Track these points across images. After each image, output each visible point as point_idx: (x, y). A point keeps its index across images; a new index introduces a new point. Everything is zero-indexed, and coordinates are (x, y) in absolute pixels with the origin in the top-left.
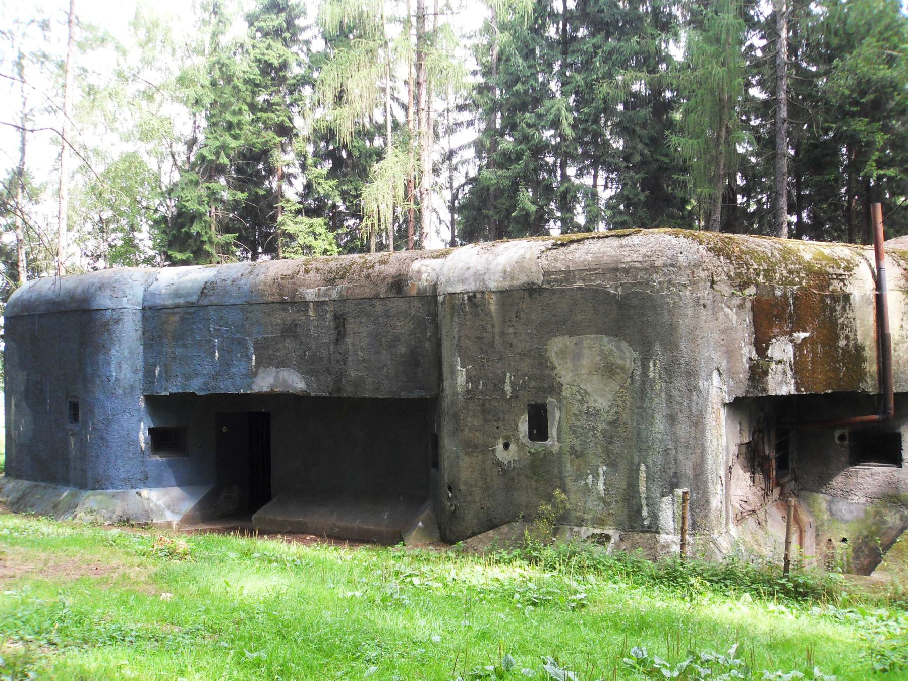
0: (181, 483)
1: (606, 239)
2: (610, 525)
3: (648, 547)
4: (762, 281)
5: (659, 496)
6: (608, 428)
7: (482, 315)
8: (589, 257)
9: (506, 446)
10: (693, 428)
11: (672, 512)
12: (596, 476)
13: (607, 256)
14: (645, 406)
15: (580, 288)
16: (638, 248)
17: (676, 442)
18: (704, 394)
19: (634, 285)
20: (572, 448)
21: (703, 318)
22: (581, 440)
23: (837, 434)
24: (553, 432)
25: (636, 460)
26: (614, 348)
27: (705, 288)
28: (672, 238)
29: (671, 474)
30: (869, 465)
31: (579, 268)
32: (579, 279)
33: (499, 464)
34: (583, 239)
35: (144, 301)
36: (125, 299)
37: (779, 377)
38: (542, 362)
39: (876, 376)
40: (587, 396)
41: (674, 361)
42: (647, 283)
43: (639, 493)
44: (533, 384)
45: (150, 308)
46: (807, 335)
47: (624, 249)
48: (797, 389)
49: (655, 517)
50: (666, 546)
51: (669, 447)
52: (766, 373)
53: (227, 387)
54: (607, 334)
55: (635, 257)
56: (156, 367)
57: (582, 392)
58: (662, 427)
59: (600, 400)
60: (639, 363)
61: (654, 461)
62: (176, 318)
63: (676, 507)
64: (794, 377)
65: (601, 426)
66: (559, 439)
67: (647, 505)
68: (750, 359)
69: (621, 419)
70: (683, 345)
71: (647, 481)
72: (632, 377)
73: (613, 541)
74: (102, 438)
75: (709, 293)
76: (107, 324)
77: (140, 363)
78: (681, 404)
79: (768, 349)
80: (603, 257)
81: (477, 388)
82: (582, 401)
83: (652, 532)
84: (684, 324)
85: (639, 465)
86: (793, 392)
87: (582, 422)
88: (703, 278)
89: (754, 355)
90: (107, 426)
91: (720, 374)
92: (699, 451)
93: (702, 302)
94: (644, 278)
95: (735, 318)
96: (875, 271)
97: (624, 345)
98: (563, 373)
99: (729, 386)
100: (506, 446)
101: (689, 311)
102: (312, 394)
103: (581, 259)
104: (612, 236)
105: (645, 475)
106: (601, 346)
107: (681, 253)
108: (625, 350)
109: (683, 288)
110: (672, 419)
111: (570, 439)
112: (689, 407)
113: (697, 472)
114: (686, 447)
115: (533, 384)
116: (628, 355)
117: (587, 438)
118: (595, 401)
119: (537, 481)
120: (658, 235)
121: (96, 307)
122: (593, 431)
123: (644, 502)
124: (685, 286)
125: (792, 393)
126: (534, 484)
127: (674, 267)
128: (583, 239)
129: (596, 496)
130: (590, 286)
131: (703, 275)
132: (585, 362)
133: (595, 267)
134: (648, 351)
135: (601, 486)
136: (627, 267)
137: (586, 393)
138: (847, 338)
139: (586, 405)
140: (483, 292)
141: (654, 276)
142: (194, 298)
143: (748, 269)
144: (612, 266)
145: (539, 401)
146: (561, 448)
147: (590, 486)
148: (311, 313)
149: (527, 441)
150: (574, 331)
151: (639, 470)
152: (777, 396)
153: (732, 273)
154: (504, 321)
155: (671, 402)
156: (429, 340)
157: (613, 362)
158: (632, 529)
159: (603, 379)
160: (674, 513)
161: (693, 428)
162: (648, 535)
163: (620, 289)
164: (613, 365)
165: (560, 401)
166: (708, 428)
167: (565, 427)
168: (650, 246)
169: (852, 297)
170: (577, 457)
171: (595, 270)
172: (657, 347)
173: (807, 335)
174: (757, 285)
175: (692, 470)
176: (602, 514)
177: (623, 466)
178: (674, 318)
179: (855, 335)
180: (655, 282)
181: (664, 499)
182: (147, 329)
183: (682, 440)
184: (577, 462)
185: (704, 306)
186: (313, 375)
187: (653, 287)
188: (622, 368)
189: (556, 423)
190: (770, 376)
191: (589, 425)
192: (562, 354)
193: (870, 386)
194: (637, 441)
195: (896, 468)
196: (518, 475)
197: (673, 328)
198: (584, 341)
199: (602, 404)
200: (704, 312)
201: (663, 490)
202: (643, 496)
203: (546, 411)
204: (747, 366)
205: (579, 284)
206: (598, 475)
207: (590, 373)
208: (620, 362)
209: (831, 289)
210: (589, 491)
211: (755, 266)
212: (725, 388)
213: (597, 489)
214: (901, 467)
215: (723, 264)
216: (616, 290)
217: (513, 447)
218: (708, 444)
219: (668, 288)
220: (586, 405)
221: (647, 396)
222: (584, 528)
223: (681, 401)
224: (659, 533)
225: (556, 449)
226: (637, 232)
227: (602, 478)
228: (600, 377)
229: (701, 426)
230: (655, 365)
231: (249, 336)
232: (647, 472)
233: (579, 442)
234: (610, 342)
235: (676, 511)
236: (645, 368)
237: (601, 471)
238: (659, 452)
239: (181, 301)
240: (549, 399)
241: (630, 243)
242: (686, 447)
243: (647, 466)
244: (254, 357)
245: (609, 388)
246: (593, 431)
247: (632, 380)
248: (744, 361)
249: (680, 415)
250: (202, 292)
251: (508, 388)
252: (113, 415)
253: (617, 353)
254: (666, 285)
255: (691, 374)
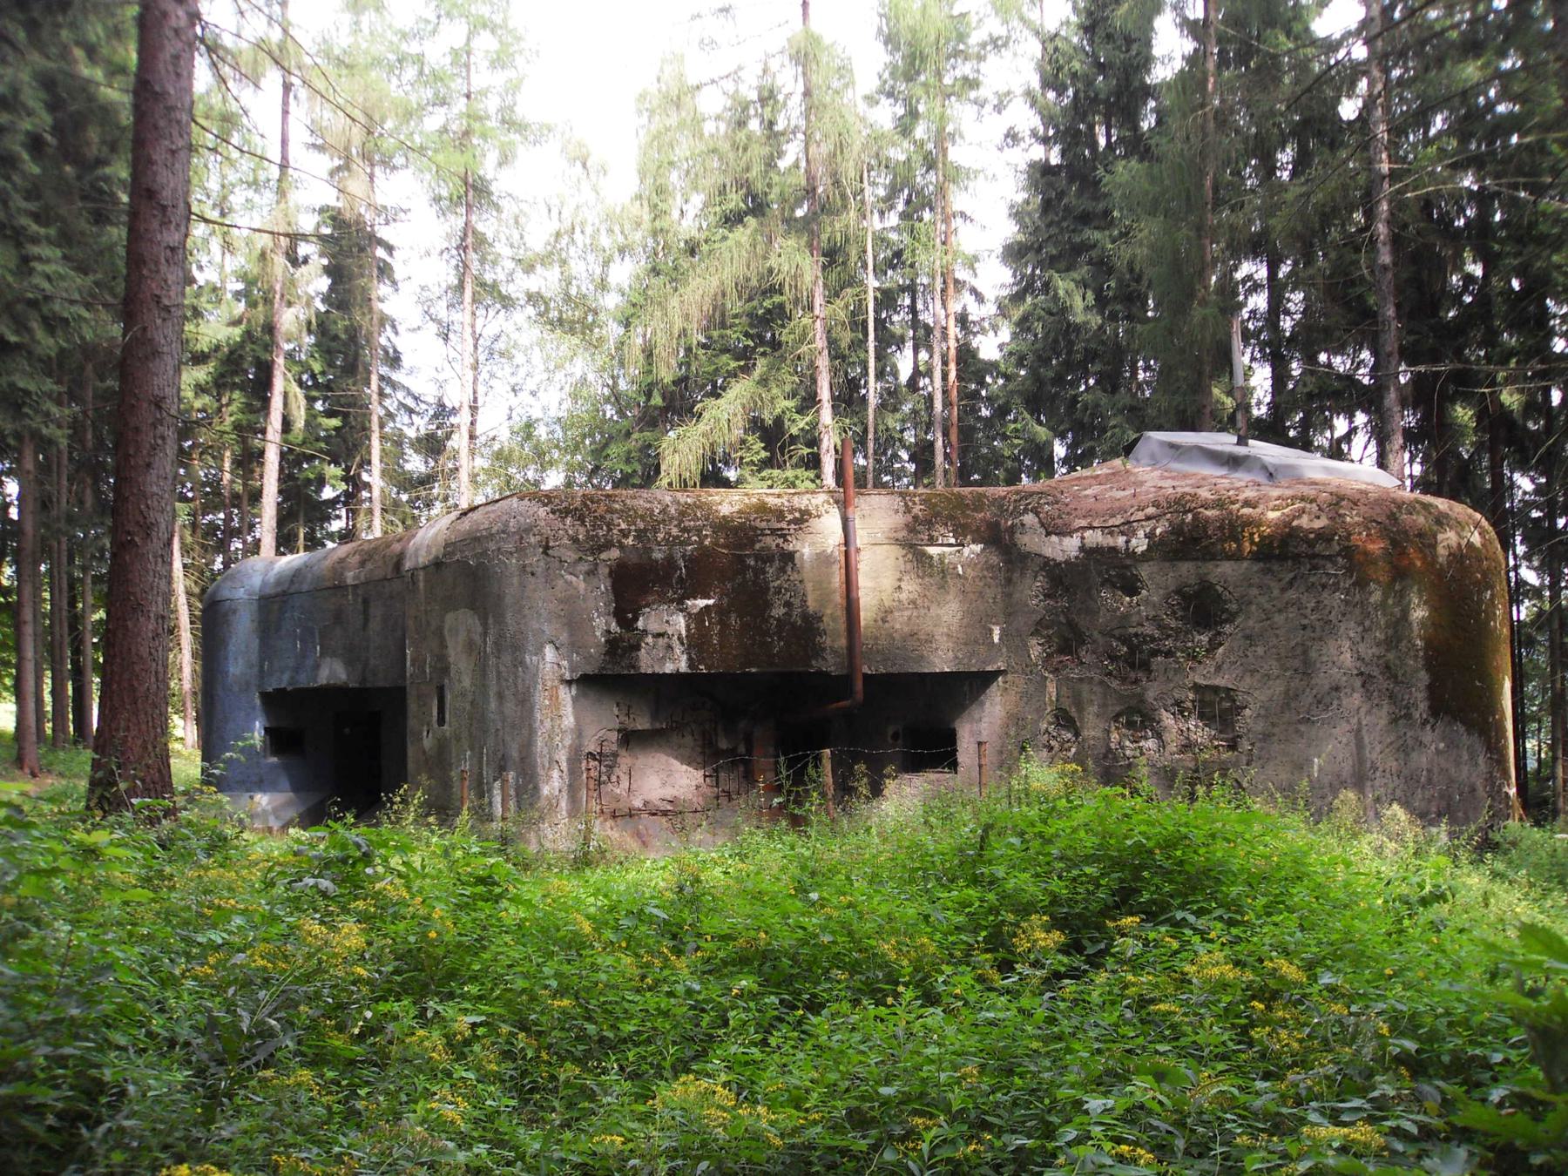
0: (296, 788)
41: (501, 636)
46: (711, 602)
53: (304, 681)
68: (608, 632)
76: (226, 615)
77: (254, 658)
84: (511, 590)
89: (614, 627)
92: (525, 732)
95: (582, 586)
99: (571, 662)
101: (515, 580)
110: (500, 696)
138: (788, 604)
143: (610, 530)
152: (654, 675)
173: (711, 602)
174: (622, 547)
197: (500, 598)
200: (531, 579)
209: (757, 546)
255: (517, 648)
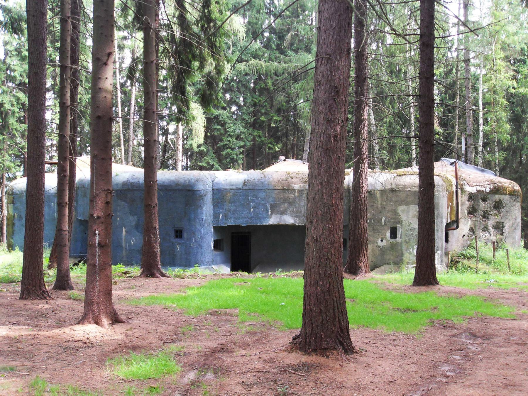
7: (374, 198)
9: (382, 241)
12: (413, 249)
20: (405, 241)
24: (399, 235)
33: (379, 247)
35: (213, 186)
36: (207, 186)
38: (395, 213)
44: (392, 221)
45: (217, 190)
56: (220, 214)
62: (231, 194)
66: (401, 238)
70: (440, 209)
74: (199, 245)
81: (371, 222)
87: (409, 232)
90: (202, 240)
98: (403, 217)
100: (382, 241)
102: (297, 225)
111: (405, 238)
115: (392, 221)
119: (393, 252)
121: (197, 189)
126: (392, 253)
137: (411, 223)
140: (374, 190)
142: (241, 186)
145: (394, 226)
146: (402, 241)
148: (296, 194)
149: (389, 239)
150: (407, 204)
154: (382, 200)
156: (346, 205)
165: (402, 226)
167: (403, 234)
170: (407, 243)
182: (215, 198)
184: (407, 244)
186: (297, 218)
189: (400, 233)
192: (403, 211)
196: (386, 250)
203: (396, 229)
205: (409, 189)
207: (412, 217)
217: (384, 241)
225: (400, 241)
231: (268, 202)
239: (234, 187)
240: (398, 225)
244: (270, 211)
250: (244, 184)
251: (383, 222)
252: (204, 235)
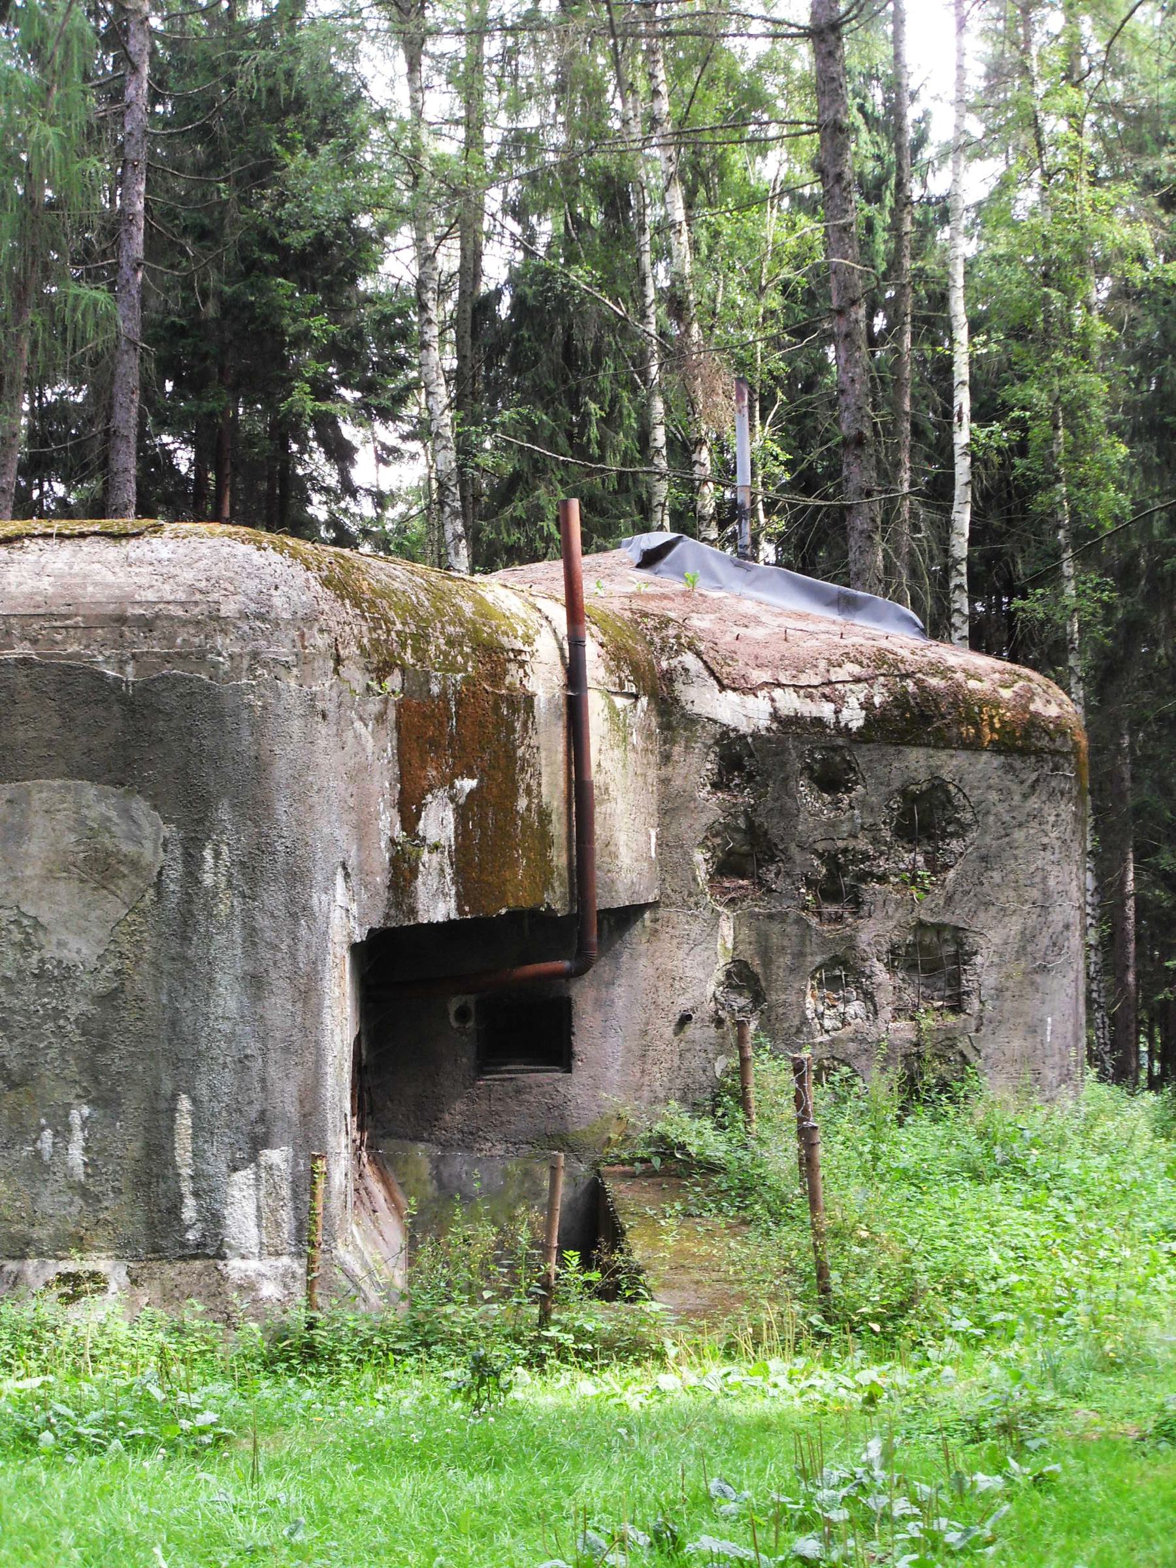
1: (83, 543)
2: (100, 1249)
3: (205, 1292)
4: (411, 661)
5: (224, 1169)
6: (92, 1010)
8: (46, 584)
10: (299, 1005)
11: (254, 1206)
12: (63, 1132)
13: (96, 584)
14: (190, 953)
15: (25, 662)
16: (177, 571)
17: (263, 1039)
18: (321, 920)
19: (167, 658)
21: (322, 743)
22: (22, 1044)
23: (453, 1005)
25: (167, 1087)
26: (113, 814)
27: (326, 674)
28: (249, 548)
29: (254, 1115)
30: (509, 1072)
31: (21, 611)
32: (23, 638)
34: (19, 537)
37: (433, 882)
39: (566, 874)
40: (41, 934)
41: (262, 848)
42: (202, 656)
43: (175, 1167)
47: (135, 569)
48: (460, 909)
49: (214, 1220)
50: (247, 1287)
51: (249, 1052)
52: (414, 872)
54: (93, 778)
55: (167, 591)
57: (26, 922)
58: (232, 1005)
59: (74, 943)
60: (178, 853)
61: (211, 1087)
63: (262, 1193)
64: (454, 882)
65: (79, 1007)
67: (196, 1194)
68: (392, 841)
69: (128, 988)
70: (281, 807)
71: (194, 1137)
72: (158, 886)
73: (113, 1287)
75: (331, 686)
78: (276, 948)
79: (419, 818)
80: (84, 586)
82: (27, 946)
83: (208, 1257)
85: (174, 1097)
86: (454, 915)
88: (323, 649)
89: (400, 835)
91: (347, 876)
93: (320, 705)
94: (191, 644)
95: (370, 744)
96: (566, 646)
97: (140, 806)
103: (26, 589)
104: (95, 534)
105: (189, 1122)
106: (79, 807)
107: (276, 588)
108: (144, 822)
109: (282, 672)
110: (255, 983)
112: (293, 957)
113: (307, 1109)
114: (286, 1050)
116: (148, 830)
117: (40, 1037)
118: (61, 944)
120: (216, 542)
122: (55, 1020)
123: (186, 1187)
124: (287, 667)
125: (452, 917)
127: (264, 621)
128: (19, 537)
129: (63, 1182)
130: (51, 656)
131: (322, 641)
132: (35, 847)
133: (64, 610)
134: (200, 821)
135: (76, 1155)
136: (149, 614)
137: (37, 924)
139: (36, 956)
141: (219, 640)
143: (389, 631)
144: (110, 609)
147: (46, 1157)
151: (175, 1110)
152: (430, 924)
153: (365, 641)
155: (254, 944)
157: (111, 848)
158: (157, 1252)
159: (82, 891)
160: (259, 1208)
161: (299, 1005)
162: (198, 1264)
163: (129, 668)
164: (109, 854)
166: (327, 1003)
168: (201, 565)
169: (536, 699)
171: (67, 617)
172: (224, 813)
175: (297, 1104)
176: (78, 1224)
177: (133, 1102)
178: (264, 741)
179: (539, 785)
180: (220, 655)
181: (238, 1177)
183: (278, 1034)
185: (324, 717)
187: (215, 665)
188: (135, 865)
190: (420, 879)
191: (43, 1005)
193: (556, 900)
194: (170, 1041)
195: (560, 1075)
197: (261, 766)
198: (36, 796)
199: (79, 951)
200: (322, 728)
201: (233, 1154)
202: (186, 1171)
204: (387, 855)
206: (69, 1128)
207: (49, 876)
208: (127, 848)
210: (46, 1168)
211: (399, 627)
212: (354, 908)
213: (65, 1164)
214: (570, 1071)
215: (350, 619)
216: (121, 670)
218: (327, 1041)
219: (251, 669)
220: (36, 956)
221: (196, 931)
222: (32, 1264)
223: (277, 942)
224: (223, 1257)
226: (157, 530)
227: (78, 1136)
228: (75, 885)
229: (314, 1000)
230: (217, 855)
232: (196, 1116)
233: (18, 1050)
234: (101, 797)
235: (263, 1202)
236: (192, 863)
237: (75, 1118)
238: (225, 1065)
241: (149, 556)
242: (286, 1050)
243: (194, 1101)
245: (98, 912)
246: (55, 1020)
247: (159, 893)
248: (383, 845)
249: (274, 975)
253: (120, 827)
254: (245, 664)
